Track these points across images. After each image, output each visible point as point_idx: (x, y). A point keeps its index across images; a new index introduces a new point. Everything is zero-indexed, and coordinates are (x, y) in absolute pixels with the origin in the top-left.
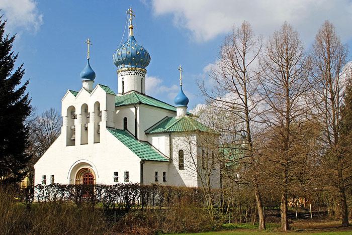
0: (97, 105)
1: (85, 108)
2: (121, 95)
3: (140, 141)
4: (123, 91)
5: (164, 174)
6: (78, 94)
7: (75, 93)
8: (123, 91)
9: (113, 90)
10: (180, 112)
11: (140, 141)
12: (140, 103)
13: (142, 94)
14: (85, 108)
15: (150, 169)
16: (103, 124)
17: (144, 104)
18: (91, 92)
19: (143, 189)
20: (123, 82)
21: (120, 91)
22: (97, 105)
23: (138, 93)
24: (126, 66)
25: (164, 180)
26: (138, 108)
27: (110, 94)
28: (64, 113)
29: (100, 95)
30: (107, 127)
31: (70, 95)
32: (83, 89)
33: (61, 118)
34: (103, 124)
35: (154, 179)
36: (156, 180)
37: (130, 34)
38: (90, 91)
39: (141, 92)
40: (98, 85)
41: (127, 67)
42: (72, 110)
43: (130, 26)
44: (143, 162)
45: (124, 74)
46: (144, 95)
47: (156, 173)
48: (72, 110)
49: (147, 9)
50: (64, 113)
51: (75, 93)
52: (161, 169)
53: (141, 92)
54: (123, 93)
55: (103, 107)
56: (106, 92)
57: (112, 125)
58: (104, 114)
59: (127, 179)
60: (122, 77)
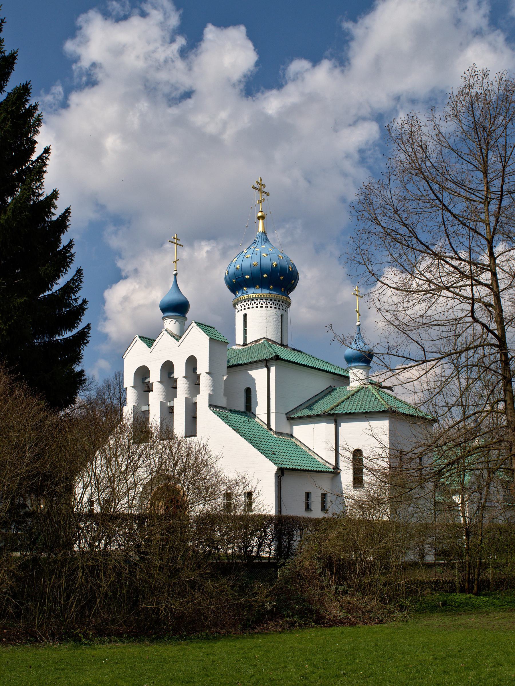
0: (192, 362)
1: (168, 368)
2: (240, 348)
3: (277, 433)
4: (245, 338)
5: (324, 496)
6: (155, 343)
7: (149, 342)
8: (245, 338)
9: (224, 336)
10: (357, 376)
11: (277, 433)
12: (277, 358)
13: (282, 345)
14: (168, 368)
15: (296, 488)
16: (202, 400)
17: (284, 360)
18: (180, 337)
19: (283, 525)
20: (294, 349)
21: (239, 340)
22: (192, 362)
23: (275, 343)
24: (251, 290)
25: (324, 508)
26: (273, 369)
27: (218, 343)
28: (129, 381)
29: (197, 343)
30: (210, 405)
31: (139, 345)
32: (164, 332)
33: (122, 391)
34: (202, 400)
35: (304, 506)
36: (308, 508)
37: (261, 229)
38: (178, 338)
39: (280, 343)
40: (194, 324)
41: (253, 292)
42: (143, 373)
43: (260, 214)
44: (281, 473)
45: (251, 306)
46: (286, 346)
47: (308, 495)
48: (143, 373)
49: (1, 103)
50: (129, 381)
51: (149, 342)
52: (318, 488)
53: (280, 343)
54: (245, 344)
55: (203, 367)
56: (209, 338)
57: (222, 402)
58: (205, 382)
59: (249, 504)
60: (244, 312)
